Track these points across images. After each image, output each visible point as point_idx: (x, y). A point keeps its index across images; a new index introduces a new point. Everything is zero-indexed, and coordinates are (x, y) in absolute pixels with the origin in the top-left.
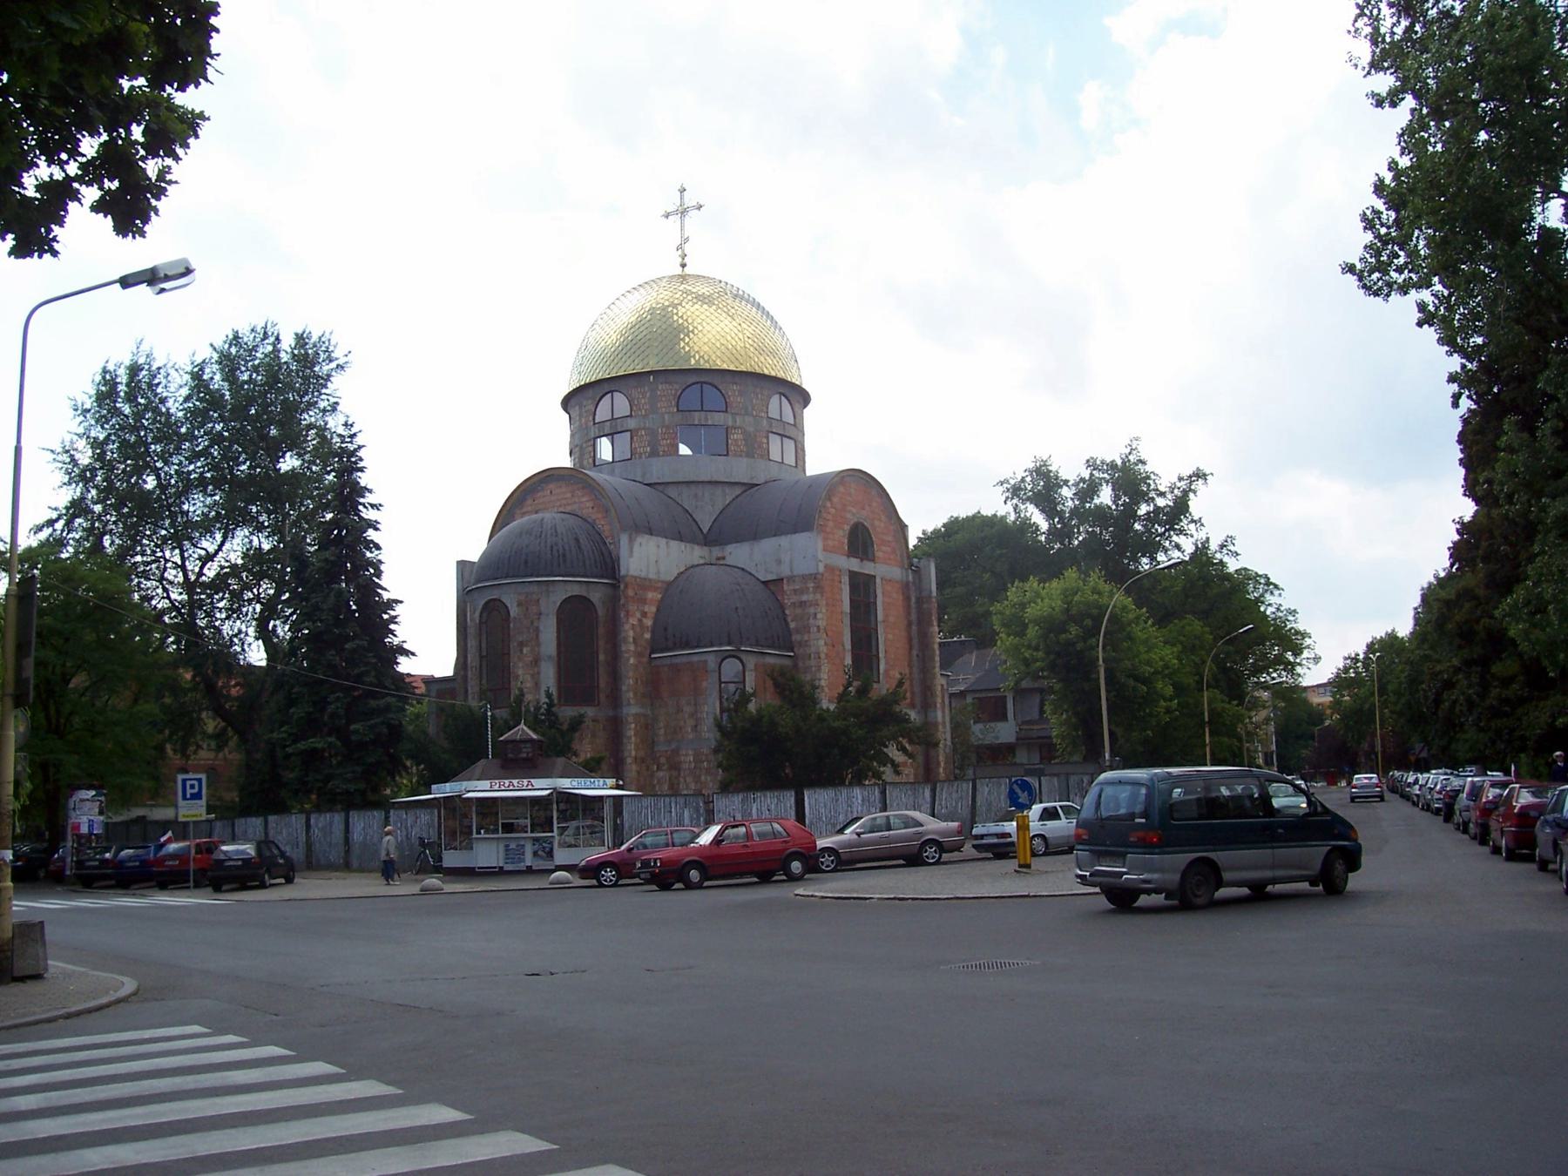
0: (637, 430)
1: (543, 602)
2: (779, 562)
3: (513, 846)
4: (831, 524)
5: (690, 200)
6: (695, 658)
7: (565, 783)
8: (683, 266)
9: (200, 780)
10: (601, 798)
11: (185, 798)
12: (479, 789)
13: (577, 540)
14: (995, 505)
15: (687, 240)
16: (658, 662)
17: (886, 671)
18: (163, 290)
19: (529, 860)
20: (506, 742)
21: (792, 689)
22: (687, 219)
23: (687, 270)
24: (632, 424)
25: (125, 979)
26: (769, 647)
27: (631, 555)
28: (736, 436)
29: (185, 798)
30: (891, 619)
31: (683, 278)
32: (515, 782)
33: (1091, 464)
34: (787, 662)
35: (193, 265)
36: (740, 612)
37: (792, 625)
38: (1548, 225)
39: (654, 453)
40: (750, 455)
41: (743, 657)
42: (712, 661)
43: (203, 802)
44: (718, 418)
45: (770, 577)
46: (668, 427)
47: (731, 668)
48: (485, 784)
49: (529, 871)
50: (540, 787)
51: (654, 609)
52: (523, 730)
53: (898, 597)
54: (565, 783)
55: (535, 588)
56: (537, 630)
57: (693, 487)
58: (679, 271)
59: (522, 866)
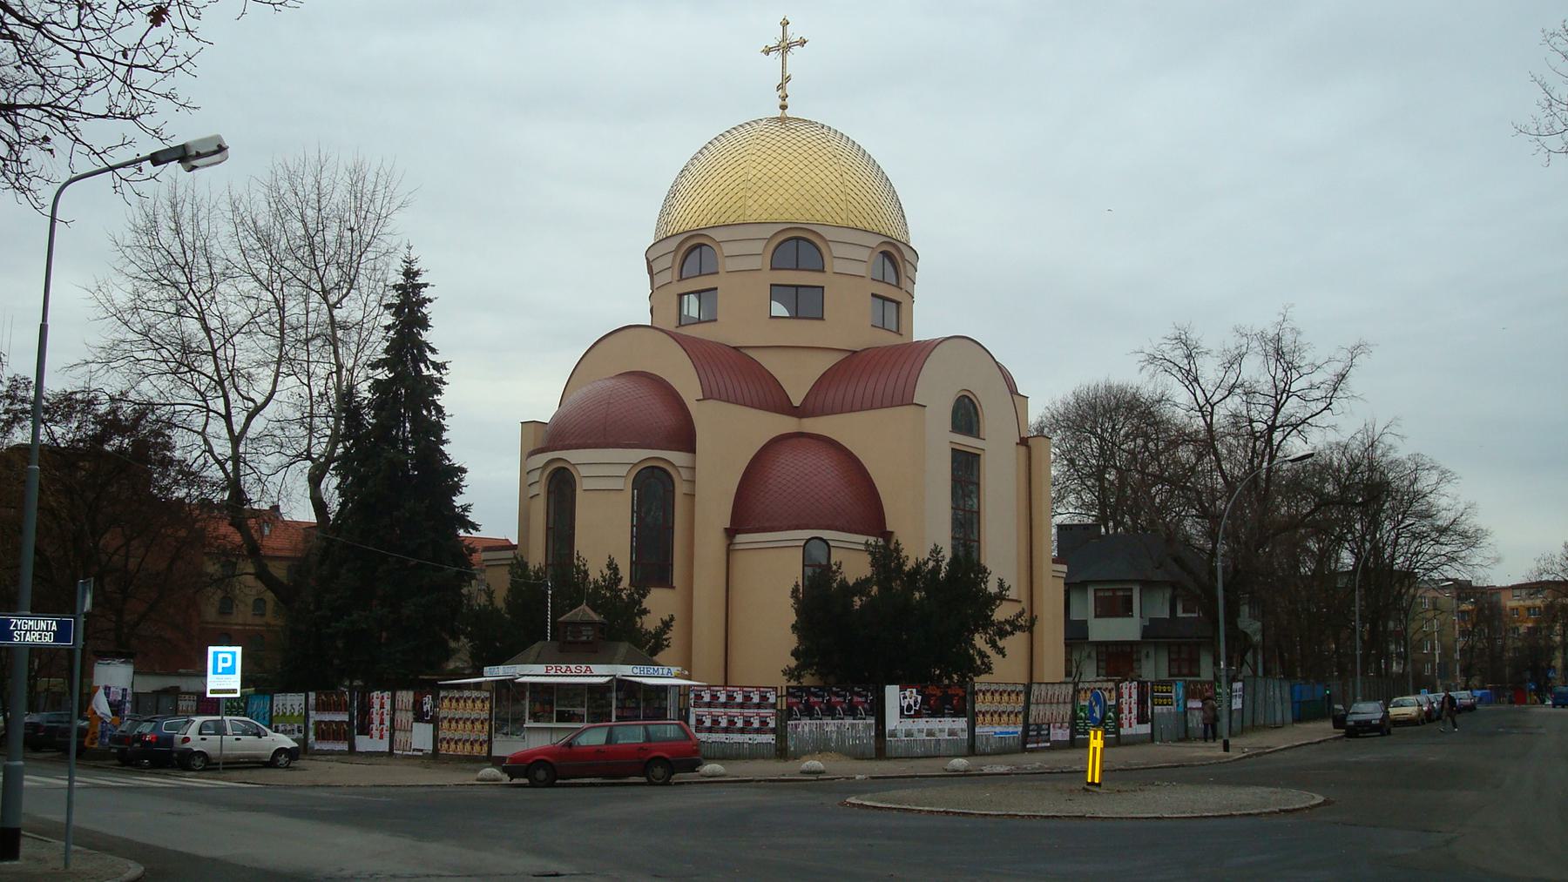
5: (794, 34)
7: (625, 671)
8: (784, 107)
10: (664, 688)
11: (215, 672)
12: (532, 673)
15: (788, 79)
18: (194, 168)
20: (566, 624)
22: (789, 56)
23: (788, 113)
25: (131, 864)
29: (215, 672)
31: (782, 120)
32: (573, 667)
35: (226, 143)
38: (23, 841)
48: (541, 669)
50: (599, 673)
52: (584, 612)
54: (625, 671)
58: (779, 113)
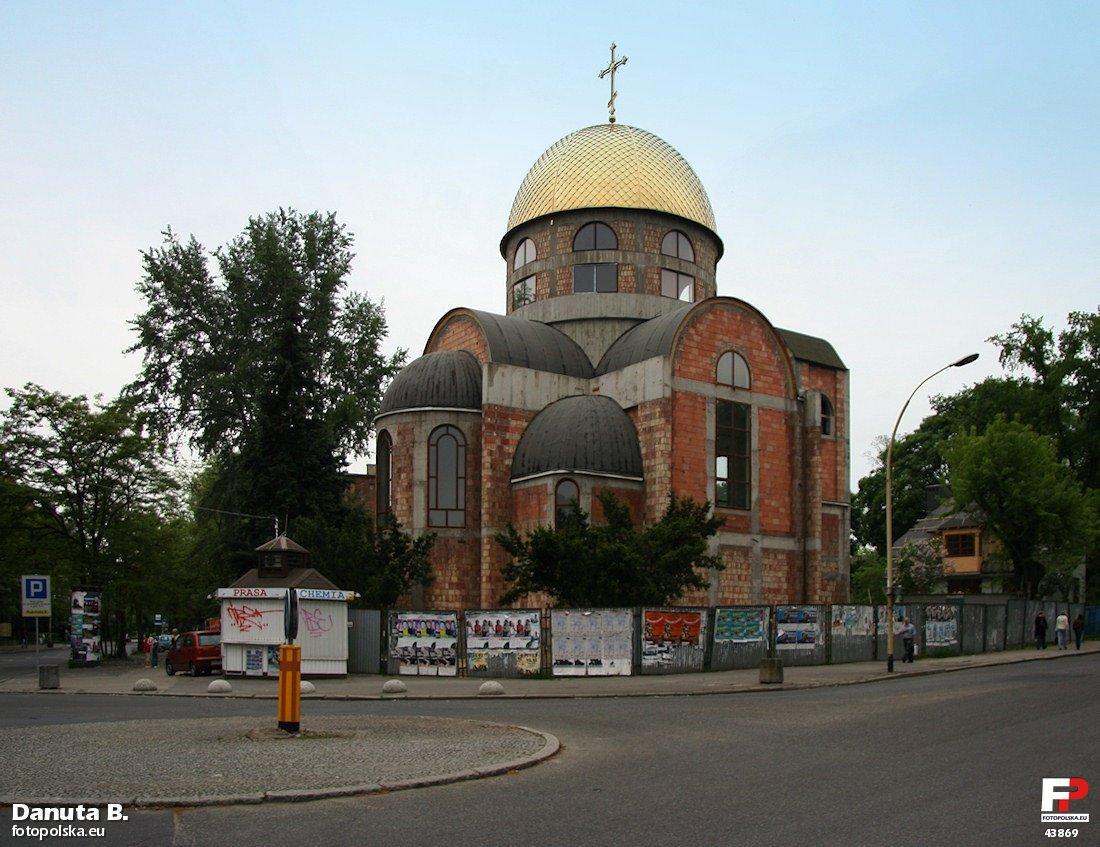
0: (540, 273)
1: (416, 431)
2: (635, 389)
3: (253, 652)
4: (695, 352)
6: (527, 485)
9: (44, 582)
11: (28, 596)
13: (453, 373)
14: (991, 368)
16: (517, 487)
17: (760, 501)
19: (265, 667)
21: (620, 513)
24: (537, 268)
26: (611, 472)
27: (491, 384)
28: (626, 273)
29: (28, 596)
30: (770, 449)
33: (1074, 318)
34: (636, 487)
36: (589, 438)
37: (643, 451)
39: (552, 294)
40: (640, 290)
41: (578, 480)
42: (550, 483)
43: (48, 600)
44: (609, 256)
45: (630, 404)
46: (564, 268)
47: (568, 490)
49: (265, 677)
51: (517, 437)
53: (779, 427)
55: (409, 419)
56: (411, 457)
57: (585, 324)
59: (259, 673)
